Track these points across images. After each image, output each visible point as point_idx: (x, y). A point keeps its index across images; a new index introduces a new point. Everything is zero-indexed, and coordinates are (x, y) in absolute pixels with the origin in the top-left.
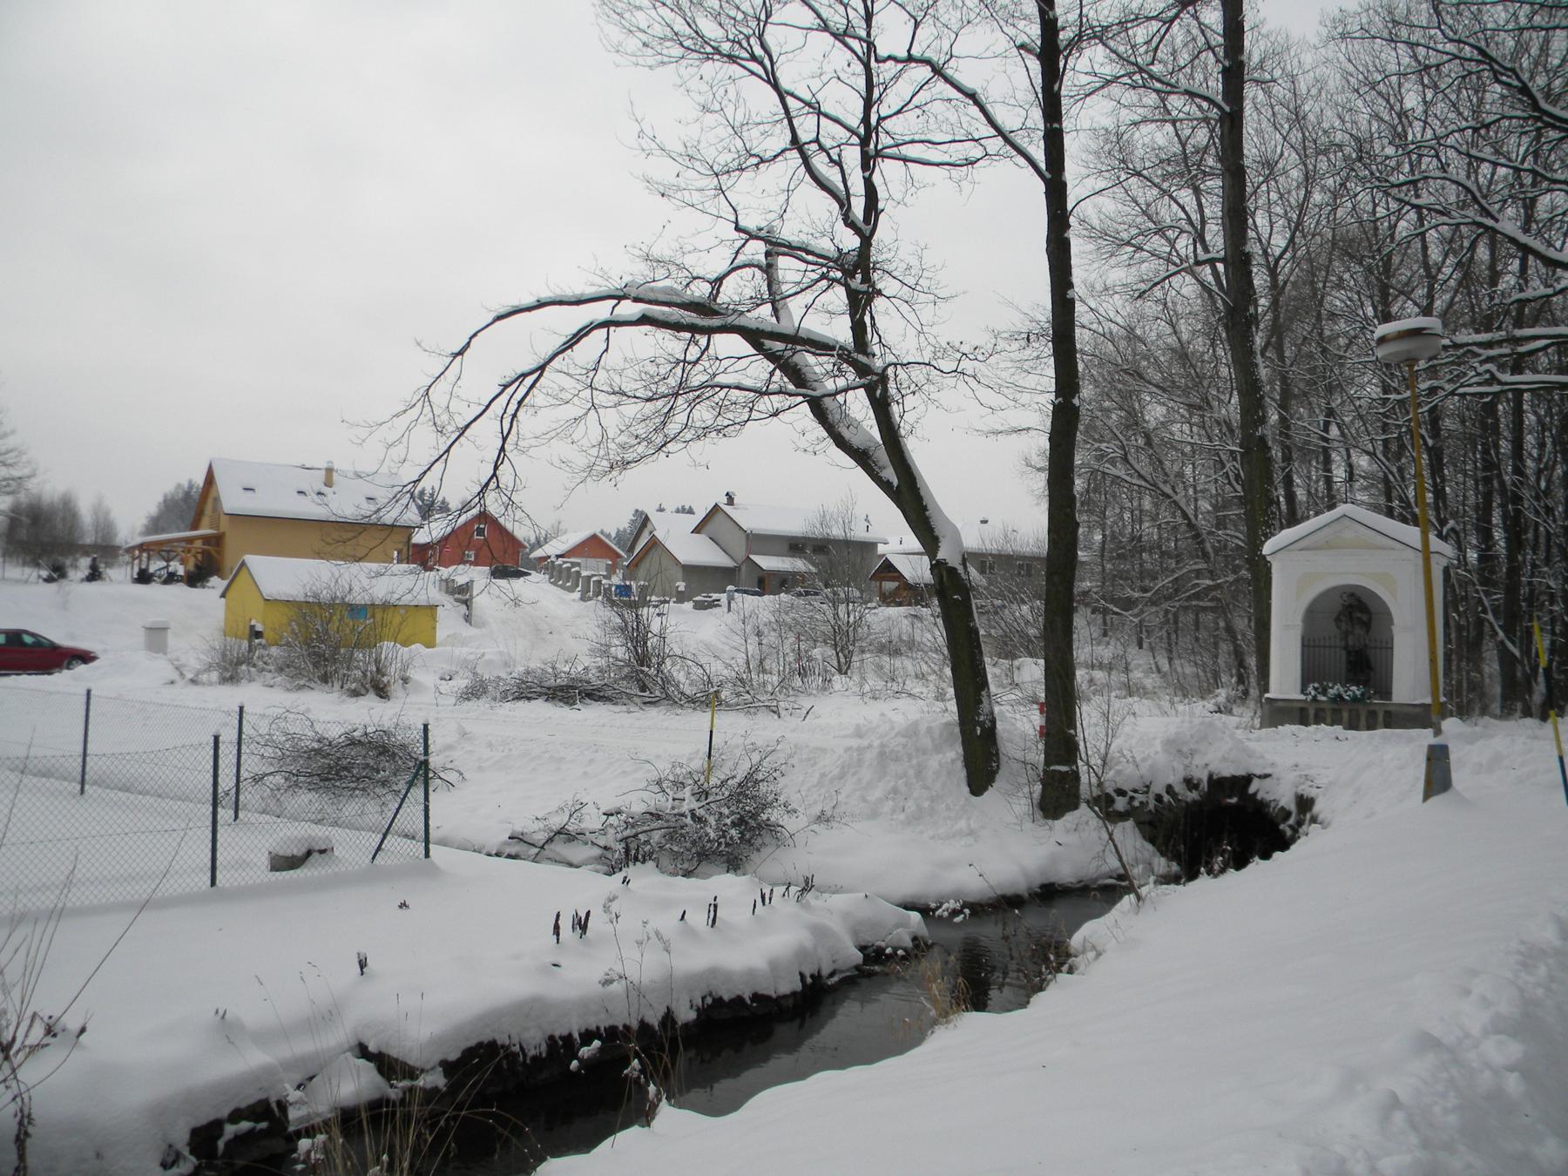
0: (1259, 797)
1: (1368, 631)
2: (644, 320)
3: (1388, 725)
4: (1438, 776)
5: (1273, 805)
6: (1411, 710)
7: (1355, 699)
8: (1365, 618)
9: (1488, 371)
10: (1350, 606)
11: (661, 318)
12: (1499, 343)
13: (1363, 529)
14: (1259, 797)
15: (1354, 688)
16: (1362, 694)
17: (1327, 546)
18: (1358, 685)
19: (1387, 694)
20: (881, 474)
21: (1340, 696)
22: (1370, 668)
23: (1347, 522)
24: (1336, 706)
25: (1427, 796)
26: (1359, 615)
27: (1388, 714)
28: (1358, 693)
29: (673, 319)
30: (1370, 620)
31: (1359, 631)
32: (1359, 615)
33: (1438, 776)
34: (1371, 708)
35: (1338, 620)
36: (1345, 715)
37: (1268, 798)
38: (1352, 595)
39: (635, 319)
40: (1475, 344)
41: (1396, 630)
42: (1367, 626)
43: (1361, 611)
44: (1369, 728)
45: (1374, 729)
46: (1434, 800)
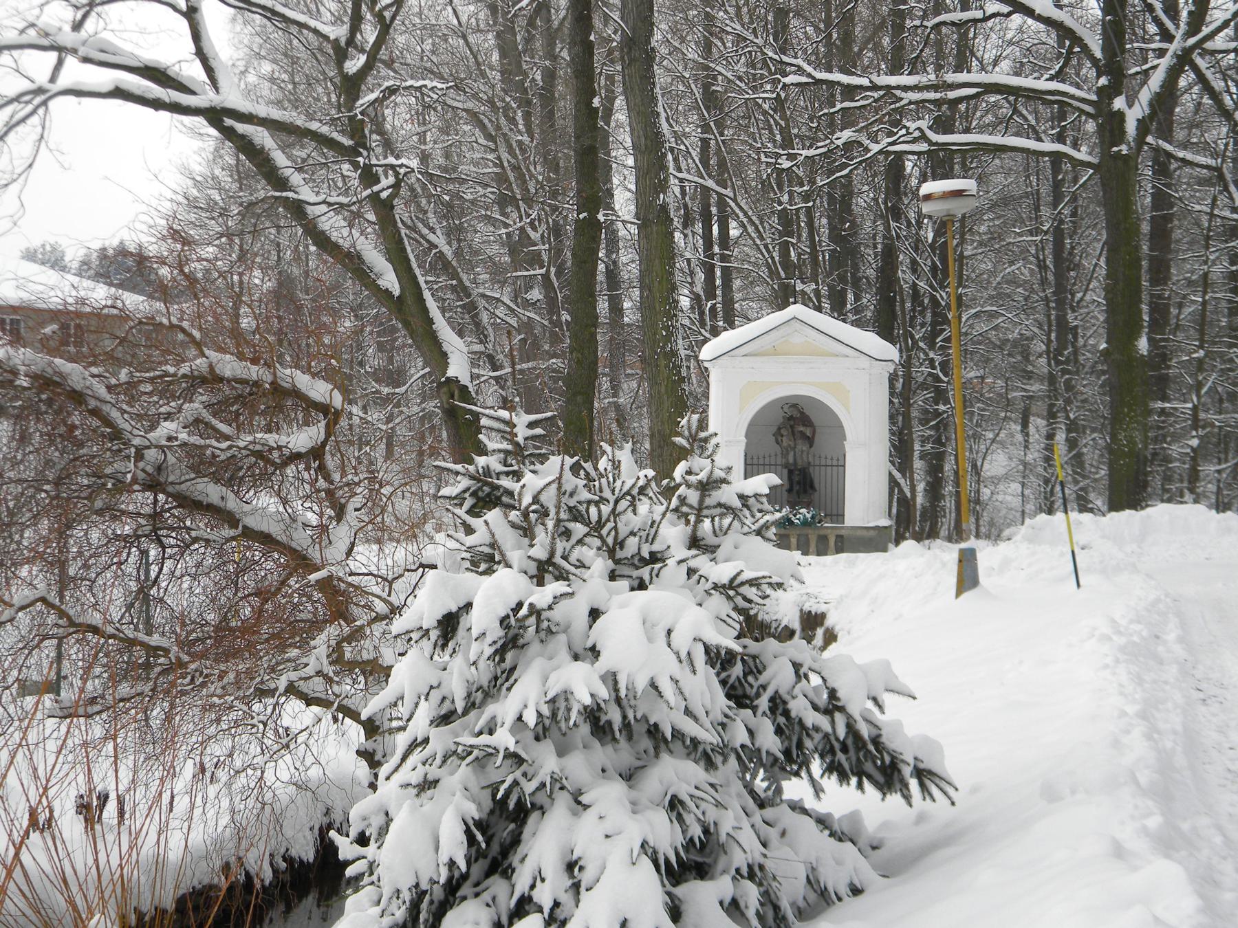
0: (760, 618)
1: (811, 446)
2: (119, 93)
3: (839, 550)
4: (967, 578)
5: (774, 625)
6: (865, 533)
7: (805, 523)
8: (808, 432)
9: (919, 129)
10: (791, 418)
11: (138, 92)
12: (927, 88)
13: (814, 333)
14: (760, 618)
15: (803, 511)
16: (813, 517)
17: (774, 352)
18: (807, 507)
19: (839, 516)
20: (380, 282)
21: (789, 520)
22: (812, 487)
23: (797, 325)
24: (783, 531)
25: (959, 592)
26: (802, 429)
27: (840, 538)
28: (808, 516)
29: (150, 96)
30: (814, 433)
31: (802, 446)
32: (802, 429)
33: (967, 578)
34: (822, 532)
35: (778, 434)
36: (794, 541)
37: (767, 618)
38: (794, 406)
39: (104, 89)
40: (898, 87)
41: (848, 446)
42: (810, 441)
43: (804, 425)
44: (819, 554)
45: (826, 554)
46: (966, 596)
